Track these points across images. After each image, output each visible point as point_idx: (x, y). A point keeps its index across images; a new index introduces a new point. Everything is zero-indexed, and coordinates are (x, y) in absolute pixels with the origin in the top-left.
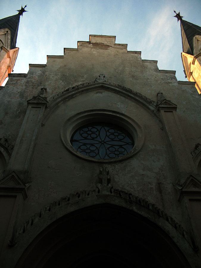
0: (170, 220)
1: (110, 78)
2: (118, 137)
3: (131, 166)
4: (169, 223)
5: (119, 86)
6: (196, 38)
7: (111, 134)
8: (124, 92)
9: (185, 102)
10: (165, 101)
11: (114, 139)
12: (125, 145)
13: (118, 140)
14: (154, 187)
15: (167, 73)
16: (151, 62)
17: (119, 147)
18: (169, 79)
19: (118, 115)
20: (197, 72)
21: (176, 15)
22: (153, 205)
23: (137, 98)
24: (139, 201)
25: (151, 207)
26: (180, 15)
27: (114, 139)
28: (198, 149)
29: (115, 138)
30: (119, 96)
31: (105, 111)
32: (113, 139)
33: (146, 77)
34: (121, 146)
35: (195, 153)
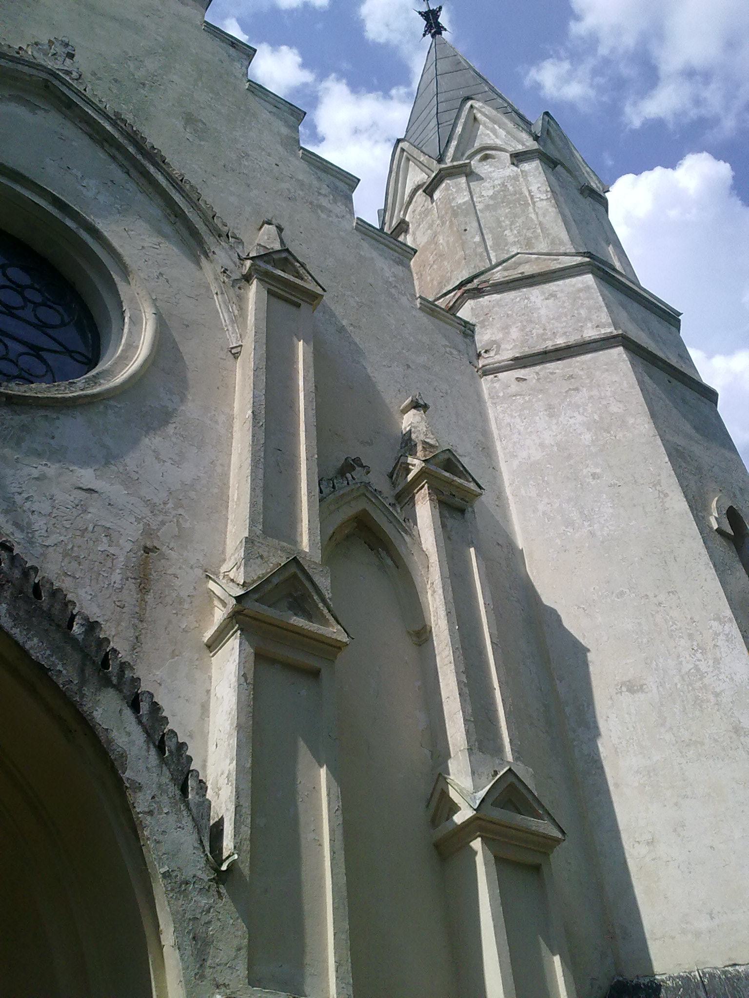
0: (144, 707)
1: (94, 74)
2: (34, 310)
3: (53, 438)
4: (140, 722)
5: (116, 120)
6: (472, 106)
7: (8, 283)
8: (131, 149)
9: (357, 299)
10: (284, 255)
11: (15, 312)
12: (55, 352)
13: (34, 320)
14: (514, 780)
15: (325, 172)
16: (281, 106)
17: (26, 350)
18: (325, 196)
19: (69, 223)
20: (430, 226)
21: (426, 13)
22: (92, 626)
23: (177, 197)
24: (37, 590)
25: (77, 629)
26: (439, 20)
27: (15, 312)
28: (350, 478)
29: (23, 308)
30: (102, 155)
31: (16, 181)
32: (32, 355)
33: (239, 146)
34: (36, 351)
35: (334, 487)
